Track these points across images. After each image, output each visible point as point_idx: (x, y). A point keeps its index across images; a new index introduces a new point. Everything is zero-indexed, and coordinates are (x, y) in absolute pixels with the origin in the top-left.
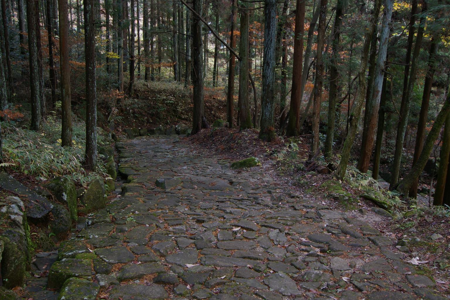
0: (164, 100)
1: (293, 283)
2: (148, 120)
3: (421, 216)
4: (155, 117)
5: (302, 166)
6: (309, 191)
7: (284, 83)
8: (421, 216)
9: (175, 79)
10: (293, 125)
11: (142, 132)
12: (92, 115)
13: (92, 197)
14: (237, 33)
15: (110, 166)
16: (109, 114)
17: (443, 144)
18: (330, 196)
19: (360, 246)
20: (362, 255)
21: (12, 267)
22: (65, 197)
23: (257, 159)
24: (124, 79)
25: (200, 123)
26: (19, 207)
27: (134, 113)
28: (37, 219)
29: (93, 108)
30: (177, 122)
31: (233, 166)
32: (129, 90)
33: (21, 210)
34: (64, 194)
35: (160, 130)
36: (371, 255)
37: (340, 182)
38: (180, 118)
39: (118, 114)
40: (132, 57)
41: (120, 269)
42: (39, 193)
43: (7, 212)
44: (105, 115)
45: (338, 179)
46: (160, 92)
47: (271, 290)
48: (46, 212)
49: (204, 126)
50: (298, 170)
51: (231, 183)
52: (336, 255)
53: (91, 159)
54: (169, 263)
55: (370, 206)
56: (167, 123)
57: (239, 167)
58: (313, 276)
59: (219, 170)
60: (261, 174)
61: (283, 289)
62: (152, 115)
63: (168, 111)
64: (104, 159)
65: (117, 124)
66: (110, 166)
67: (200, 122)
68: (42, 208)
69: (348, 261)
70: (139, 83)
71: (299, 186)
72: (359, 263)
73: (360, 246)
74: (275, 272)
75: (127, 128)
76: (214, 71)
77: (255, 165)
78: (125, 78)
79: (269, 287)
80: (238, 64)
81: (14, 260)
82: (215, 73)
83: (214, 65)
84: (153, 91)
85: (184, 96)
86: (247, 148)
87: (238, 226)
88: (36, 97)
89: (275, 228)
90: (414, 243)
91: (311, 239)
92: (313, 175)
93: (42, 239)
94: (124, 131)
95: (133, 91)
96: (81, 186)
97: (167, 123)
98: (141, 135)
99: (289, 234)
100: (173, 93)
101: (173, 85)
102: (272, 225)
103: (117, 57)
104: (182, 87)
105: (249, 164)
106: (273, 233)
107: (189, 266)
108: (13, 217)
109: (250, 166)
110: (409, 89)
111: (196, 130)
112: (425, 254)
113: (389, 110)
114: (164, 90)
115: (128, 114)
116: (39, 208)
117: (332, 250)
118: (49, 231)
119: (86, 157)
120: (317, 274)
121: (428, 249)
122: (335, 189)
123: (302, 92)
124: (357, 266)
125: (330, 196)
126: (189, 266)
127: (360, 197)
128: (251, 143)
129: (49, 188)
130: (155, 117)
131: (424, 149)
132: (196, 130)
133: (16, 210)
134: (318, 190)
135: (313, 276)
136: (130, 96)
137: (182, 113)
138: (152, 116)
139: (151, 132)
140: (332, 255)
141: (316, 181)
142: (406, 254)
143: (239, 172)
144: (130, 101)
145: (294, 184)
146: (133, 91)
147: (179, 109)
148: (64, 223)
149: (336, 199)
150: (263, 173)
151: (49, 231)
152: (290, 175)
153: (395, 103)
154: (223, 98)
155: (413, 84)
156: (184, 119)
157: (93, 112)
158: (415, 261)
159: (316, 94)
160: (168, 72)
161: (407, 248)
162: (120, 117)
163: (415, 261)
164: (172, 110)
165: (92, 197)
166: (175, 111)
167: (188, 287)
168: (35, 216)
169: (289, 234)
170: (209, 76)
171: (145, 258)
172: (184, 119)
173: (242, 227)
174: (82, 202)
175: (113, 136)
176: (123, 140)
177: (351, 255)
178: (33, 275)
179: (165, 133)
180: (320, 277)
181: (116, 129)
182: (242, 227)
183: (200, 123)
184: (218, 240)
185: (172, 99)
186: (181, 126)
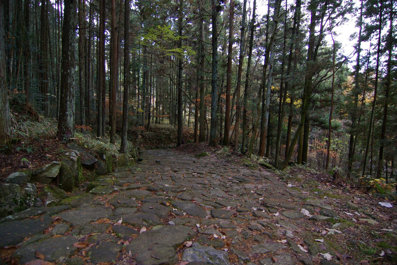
0: (164, 132)
1: (224, 193)
2: (156, 142)
3: (291, 169)
4: (160, 141)
5: (230, 154)
6: (234, 164)
7: (222, 122)
8: (291, 169)
9: (170, 123)
10: (225, 142)
11: (153, 147)
12: (125, 127)
13: (121, 163)
14: (198, 100)
15: (133, 154)
16: (137, 138)
17: (298, 154)
18: (244, 165)
19: (260, 180)
20: (261, 183)
21: (65, 178)
22: (105, 157)
23: (207, 153)
24: (145, 123)
25: (181, 141)
26: (76, 154)
27: (149, 138)
28: (88, 165)
29: (126, 123)
30: (170, 143)
31: (195, 156)
32: (148, 127)
33: (77, 155)
34: (104, 155)
35: (162, 147)
36: (266, 183)
37: (249, 159)
38: (171, 141)
39: (142, 138)
40: (149, 112)
41: (127, 185)
42: (91, 154)
43: (69, 155)
44: (135, 138)
45: (248, 157)
46: (162, 129)
47: (211, 194)
48: (93, 162)
49: (183, 143)
50: (228, 156)
51: (194, 162)
52: (247, 183)
53: (123, 149)
54: (156, 184)
55: (264, 169)
56: (165, 144)
57: (198, 157)
58: (235, 189)
59: (188, 158)
60: (210, 158)
61: (217, 194)
62: (158, 140)
63: (166, 138)
64: (130, 151)
65: (141, 143)
66: (133, 154)
67: (180, 141)
68: (91, 160)
69: (254, 185)
70: (152, 125)
71: (228, 162)
72: (260, 186)
73: (260, 180)
74: (213, 188)
75: (145, 145)
76: (189, 121)
77: (207, 155)
78: (146, 122)
79: (210, 193)
80: (200, 119)
81: (67, 174)
82: (189, 122)
83: (188, 118)
84: (159, 129)
85: (174, 131)
86: (203, 150)
87: (195, 173)
88: (100, 124)
89: (215, 174)
90: (289, 178)
91: (234, 178)
92: (235, 157)
93: (89, 175)
94: (144, 146)
95: (149, 128)
96: (116, 157)
97: (165, 144)
98: (152, 149)
99: (222, 176)
100: (168, 129)
101: (169, 126)
102: (214, 173)
103: (142, 111)
104: (173, 127)
105: (204, 155)
106: (214, 176)
107: (166, 185)
108: (71, 157)
109: (204, 156)
110: (281, 121)
111: (179, 145)
112: (294, 182)
113: (272, 136)
114: (164, 128)
115: (147, 139)
116: (89, 160)
117: (245, 181)
118: (94, 173)
119: (121, 148)
120: (237, 189)
121: (296, 180)
122: (246, 162)
123: (229, 130)
124: (259, 187)
125: (244, 165)
126: (166, 185)
127: (259, 164)
128: (205, 147)
129: (96, 152)
130: (160, 141)
131: (290, 149)
132: (179, 145)
133: (74, 155)
134: (238, 163)
135: (235, 189)
136: (148, 131)
137: (172, 139)
138: (159, 140)
139: (157, 148)
140: (245, 183)
141: (237, 159)
142: (285, 183)
143: (199, 159)
144: (148, 133)
145: (226, 162)
146: (149, 128)
147: (171, 137)
148: (102, 169)
149: (247, 166)
150: (211, 158)
151: (94, 173)
152: (224, 158)
153: (275, 132)
154: (192, 132)
155: (283, 118)
156: (173, 142)
157: (126, 125)
158: (290, 185)
159: (235, 130)
160: (167, 121)
161: (284, 180)
162: (142, 140)
163: (290, 185)
164: (168, 137)
165: (121, 163)
166: (169, 138)
167: (165, 193)
168: (87, 164)
169: (222, 176)
170: (186, 123)
171: (142, 182)
172: (173, 142)
173: (197, 173)
174: (115, 165)
175: (138, 148)
176: (143, 150)
177: (255, 183)
178: (80, 189)
179: (164, 148)
180: (239, 190)
181: (140, 145)
182: (197, 173)
183: (181, 141)
184: (184, 178)
185: (168, 132)
186: (172, 145)
